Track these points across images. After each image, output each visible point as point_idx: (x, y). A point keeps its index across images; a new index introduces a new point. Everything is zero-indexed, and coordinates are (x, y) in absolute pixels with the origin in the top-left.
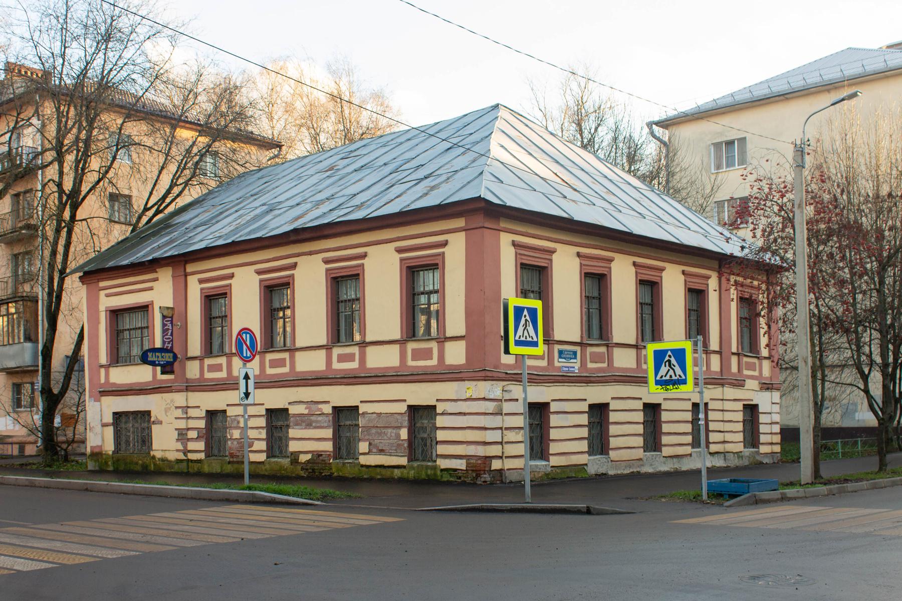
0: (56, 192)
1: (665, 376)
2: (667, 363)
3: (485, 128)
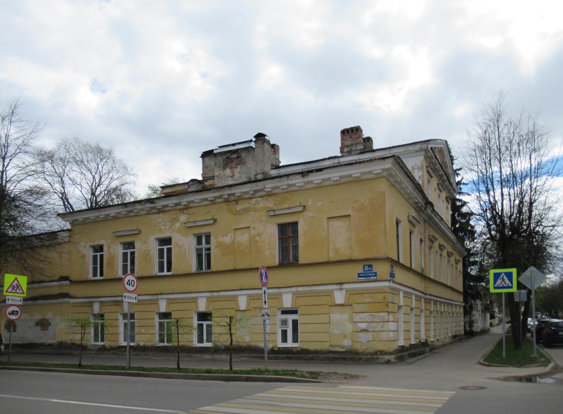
0: (178, 344)
1: (500, 284)
2: (501, 279)
3: (371, 292)
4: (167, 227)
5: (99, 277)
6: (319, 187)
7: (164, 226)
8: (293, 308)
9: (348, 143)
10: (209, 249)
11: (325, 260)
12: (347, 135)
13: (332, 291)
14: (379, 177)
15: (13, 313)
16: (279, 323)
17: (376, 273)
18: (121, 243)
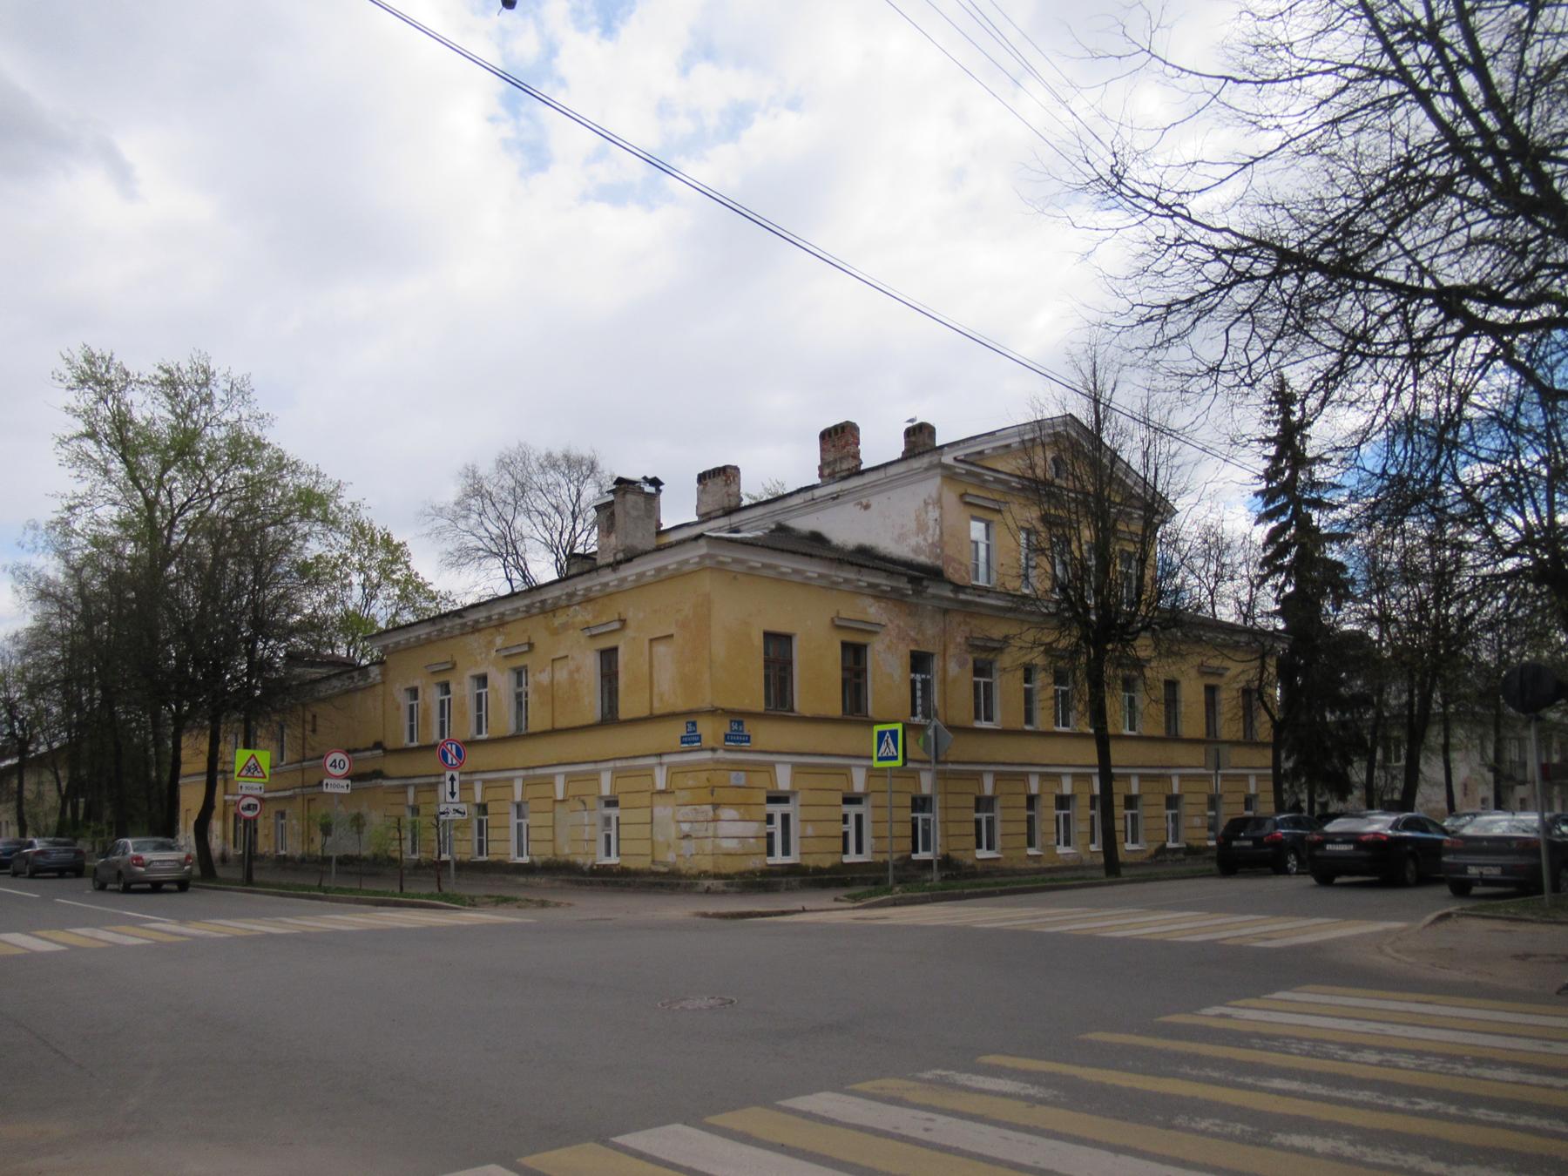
6: (641, 584)
9: (830, 458)
13: (651, 768)
14: (701, 568)
15: (248, 807)
16: (600, 823)
17: (700, 736)
18: (437, 684)
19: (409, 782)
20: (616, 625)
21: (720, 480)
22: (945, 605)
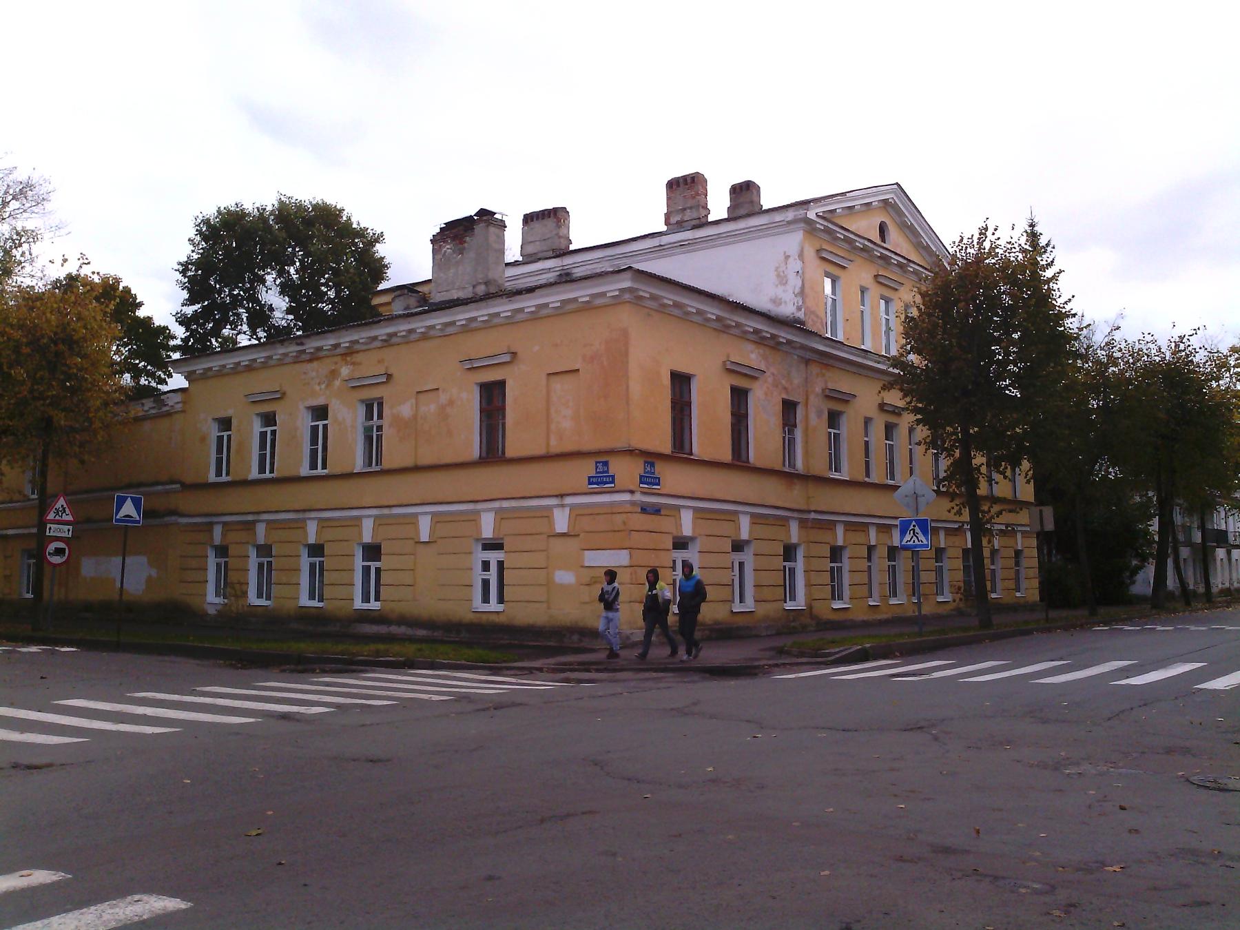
2: (912, 532)
4: (323, 386)
5: (320, 471)
6: (536, 316)
7: (319, 384)
8: (497, 539)
10: (380, 428)
11: (541, 451)
12: (676, 190)
13: (549, 508)
14: (617, 301)
17: (613, 477)
19: (215, 519)
20: (507, 358)
21: (550, 223)
22: (808, 355)
